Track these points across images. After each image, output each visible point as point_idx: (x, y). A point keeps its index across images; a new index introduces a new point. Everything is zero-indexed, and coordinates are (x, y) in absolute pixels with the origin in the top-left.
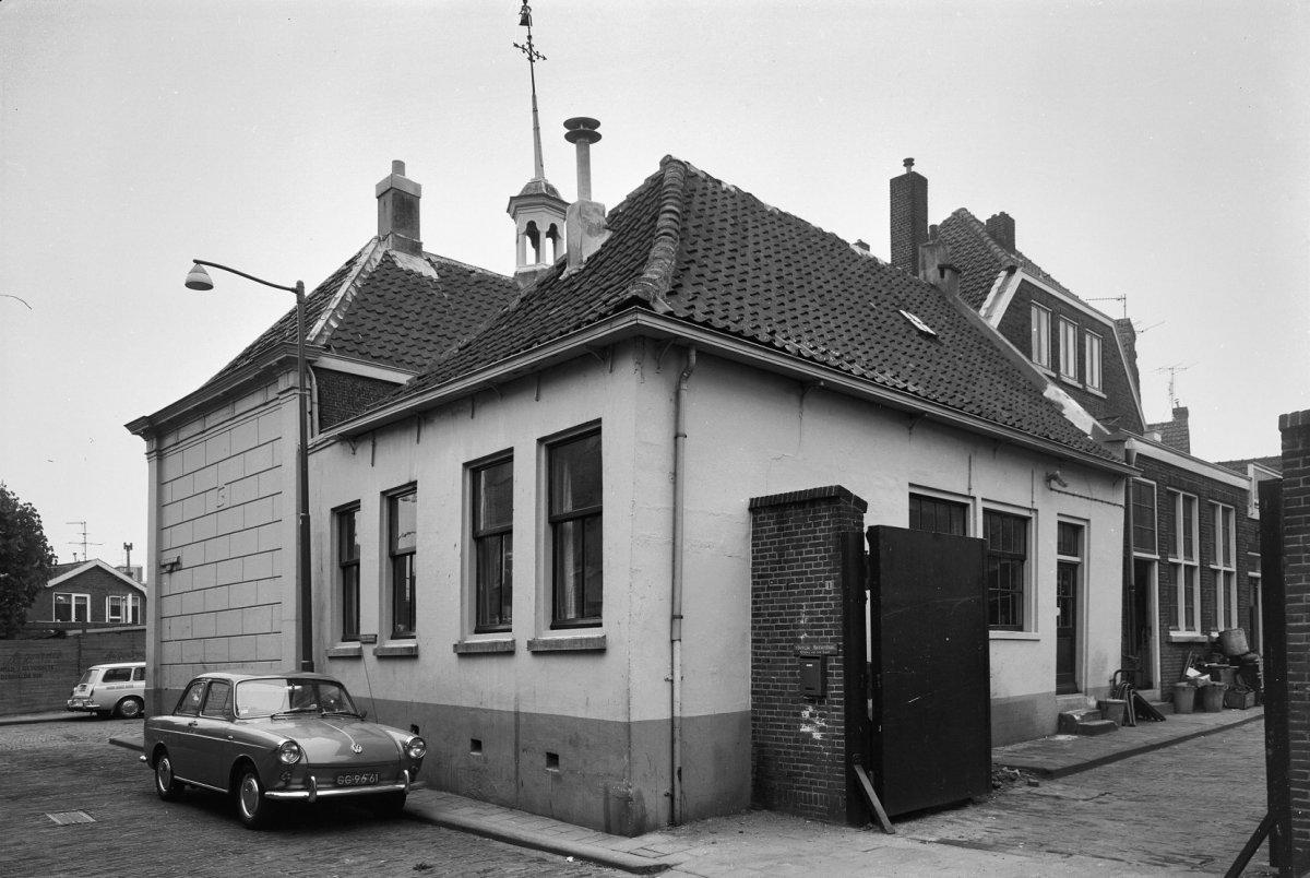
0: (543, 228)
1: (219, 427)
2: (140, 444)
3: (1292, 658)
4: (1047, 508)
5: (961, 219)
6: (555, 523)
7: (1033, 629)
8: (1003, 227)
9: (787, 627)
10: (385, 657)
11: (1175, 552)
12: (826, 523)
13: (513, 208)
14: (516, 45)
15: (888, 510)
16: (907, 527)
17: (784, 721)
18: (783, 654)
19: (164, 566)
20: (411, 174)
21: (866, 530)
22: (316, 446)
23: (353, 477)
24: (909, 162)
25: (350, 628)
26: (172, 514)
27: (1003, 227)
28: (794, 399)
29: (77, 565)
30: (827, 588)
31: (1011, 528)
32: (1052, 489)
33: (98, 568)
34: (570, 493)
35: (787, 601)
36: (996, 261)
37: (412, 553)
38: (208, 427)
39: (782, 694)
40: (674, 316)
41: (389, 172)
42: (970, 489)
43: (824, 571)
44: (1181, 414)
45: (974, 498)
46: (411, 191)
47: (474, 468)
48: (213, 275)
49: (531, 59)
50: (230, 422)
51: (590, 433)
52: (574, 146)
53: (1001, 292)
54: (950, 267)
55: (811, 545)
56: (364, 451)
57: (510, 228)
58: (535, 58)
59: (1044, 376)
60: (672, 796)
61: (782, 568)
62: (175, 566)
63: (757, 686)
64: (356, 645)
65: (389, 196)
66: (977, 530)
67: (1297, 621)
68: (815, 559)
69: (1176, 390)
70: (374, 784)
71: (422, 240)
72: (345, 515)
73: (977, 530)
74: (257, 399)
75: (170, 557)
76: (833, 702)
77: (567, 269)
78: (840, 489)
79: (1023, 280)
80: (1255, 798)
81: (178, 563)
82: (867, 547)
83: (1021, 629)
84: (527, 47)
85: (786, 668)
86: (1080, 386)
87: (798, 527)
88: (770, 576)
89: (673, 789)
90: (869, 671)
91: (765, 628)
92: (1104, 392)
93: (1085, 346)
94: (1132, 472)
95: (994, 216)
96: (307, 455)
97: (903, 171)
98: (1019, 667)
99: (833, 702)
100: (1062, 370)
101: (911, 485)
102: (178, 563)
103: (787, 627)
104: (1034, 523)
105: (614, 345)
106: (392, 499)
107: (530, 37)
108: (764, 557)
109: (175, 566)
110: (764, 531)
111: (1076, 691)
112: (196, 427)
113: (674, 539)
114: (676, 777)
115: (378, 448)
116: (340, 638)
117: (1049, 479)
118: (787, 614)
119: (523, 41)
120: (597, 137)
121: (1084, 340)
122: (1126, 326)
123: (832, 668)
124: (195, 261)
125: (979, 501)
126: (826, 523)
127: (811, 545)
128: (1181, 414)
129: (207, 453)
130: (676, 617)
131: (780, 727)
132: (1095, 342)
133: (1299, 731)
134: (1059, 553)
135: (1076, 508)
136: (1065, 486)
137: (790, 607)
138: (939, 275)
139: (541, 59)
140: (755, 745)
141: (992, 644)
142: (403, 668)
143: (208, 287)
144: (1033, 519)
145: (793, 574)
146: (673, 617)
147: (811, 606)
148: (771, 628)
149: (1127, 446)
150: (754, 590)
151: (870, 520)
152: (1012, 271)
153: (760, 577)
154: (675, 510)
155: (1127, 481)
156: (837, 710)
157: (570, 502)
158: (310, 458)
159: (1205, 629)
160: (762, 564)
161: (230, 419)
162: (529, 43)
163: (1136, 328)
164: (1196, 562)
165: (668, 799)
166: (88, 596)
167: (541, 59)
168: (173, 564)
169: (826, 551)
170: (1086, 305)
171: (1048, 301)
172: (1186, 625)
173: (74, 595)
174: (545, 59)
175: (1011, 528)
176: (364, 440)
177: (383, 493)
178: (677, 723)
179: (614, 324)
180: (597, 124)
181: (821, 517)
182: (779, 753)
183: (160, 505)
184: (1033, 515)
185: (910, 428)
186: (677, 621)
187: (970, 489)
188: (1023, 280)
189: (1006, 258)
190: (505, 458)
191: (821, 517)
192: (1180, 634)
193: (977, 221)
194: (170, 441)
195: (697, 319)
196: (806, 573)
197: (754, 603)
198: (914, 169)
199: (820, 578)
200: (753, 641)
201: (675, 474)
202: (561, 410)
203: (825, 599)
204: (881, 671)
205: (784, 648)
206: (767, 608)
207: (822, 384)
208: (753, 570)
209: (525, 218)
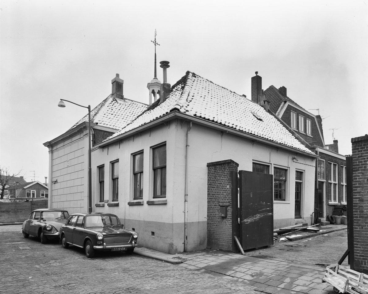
0: (156, 91)
1: (68, 145)
2: (47, 149)
3: (355, 206)
4: (293, 166)
5: (272, 88)
6: (155, 170)
7: (288, 201)
8: (283, 90)
9: (217, 198)
10: (110, 205)
11: (331, 180)
12: (227, 170)
15: (245, 165)
16: (251, 170)
17: (216, 224)
18: (216, 205)
19: (53, 182)
20: (121, 77)
21: (238, 172)
22: (93, 149)
23: (102, 158)
24: (257, 73)
25: (102, 199)
26: (55, 168)
27: (283, 90)
28: (220, 136)
29: (32, 182)
30: (227, 187)
31: (282, 172)
32: (294, 162)
33: (38, 183)
34: (159, 163)
35: (217, 191)
36: (281, 100)
37: (118, 178)
38: (65, 144)
39: (215, 216)
40: (252, 134)
41: (115, 76)
42: (270, 161)
43: (227, 183)
44: (336, 142)
45: (271, 164)
46: (121, 82)
47: (134, 155)
48: (65, 103)
50: (70, 143)
51: (163, 145)
52: (162, 69)
53: (282, 108)
54: (267, 101)
55: (223, 176)
56: (106, 150)
59: (293, 131)
60: (184, 244)
61: (215, 182)
62: (56, 182)
63: (209, 214)
64: (103, 203)
65: (115, 83)
66: (272, 172)
67: (356, 196)
68: (224, 179)
69: (334, 135)
70: (119, 247)
71: (123, 95)
72: (101, 168)
73: (272, 172)
74: (78, 137)
75: (54, 180)
76: (229, 219)
77: (160, 102)
78: (231, 160)
79: (289, 105)
80: (345, 246)
81: (57, 181)
82: (238, 176)
83: (284, 200)
84: (154, 42)
85: (216, 209)
86: (305, 134)
87: (220, 171)
88: (212, 184)
89: (185, 242)
90: (239, 210)
91: (211, 198)
92: (312, 135)
93: (306, 123)
94: (318, 157)
95: (281, 87)
96: (91, 152)
97: (255, 75)
98: (283, 212)
99: (229, 219)
100: (307, 133)
101: (253, 160)
102: (57, 181)
103: (217, 198)
104: (288, 171)
105: (170, 121)
106: (113, 163)
107: (155, 39)
108: (211, 179)
109: (56, 182)
110: (210, 172)
111: (300, 218)
112: (62, 145)
113: (186, 174)
114: (186, 239)
115: (109, 150)
117: (293, 159)
118: (217, 195)
119: (154, 40)
120: (169, 66)
121: (306, 121)
122: (319, 117)
123: (229, 209)
124: (61, 99)
125: (272, 164)
126: (227, 170)
127: (223, 176)
128: (336, 142)
129: (62, 151)
130: (186, 195)
131: (215, 225)
132: (309, 121)
133: (357, 227)
134: (296, 179)
135: (301, 167)
136: (297, 161)
137: (217, 193)
138: (264, 103)
140: (208, 230)
141: (274, 204)
142: (116, 208)
143: (64, 106)
144: (288, 170)
145: (218, 184)
146: (185, 195)
147: (223, 192)
148: (212, 198)
149: (316, 150)
150: (208, 188)
151: (239, 169)
152: (285, 102)
153: (210, 184)
154: (186, 166)
155: (316, 160)
156: (230, 221)
157: (159, 164)
158: (91, 153)
159: (339, 201)
160: (210, 181)
161: (71, 142)
163: (322, 118)
164: (337, 183)
165: (184, 244)
166: (35, 191)
168: (55, 182)
169: (227, 177)
170: (307, 111)
171: (295, 110)
172: (334, 200)
173: (31, 191)
175: (282, 172)
176: (106, 148)
177: (110, 162)
178: (186, 224)
179: (169, 115)
180: (169, 63)
181: (226, 168)
182: (214, 233)
183: (52, 166)
184: (288, 169)
185: (277, 151)
186: (186, 196)
187: (270, 161)
188: (289, 105)
189: (283, 99)
190: (141, 152)
191: (226, 168)
192: (332, 202)
193: (276, 89)
194: (55, 148)
195: (230, 126)
196: (222, 183)
197: (208, 191)
198: (258, 74)
199: (225, 185)
200: (208, 202)
201: (186, 156)
202: (156, 139)
203: (227, 190)
204: (244, 211)
205: (216, 204)
206: (211, 193)
207: (227, 132)
208: (208, 183)
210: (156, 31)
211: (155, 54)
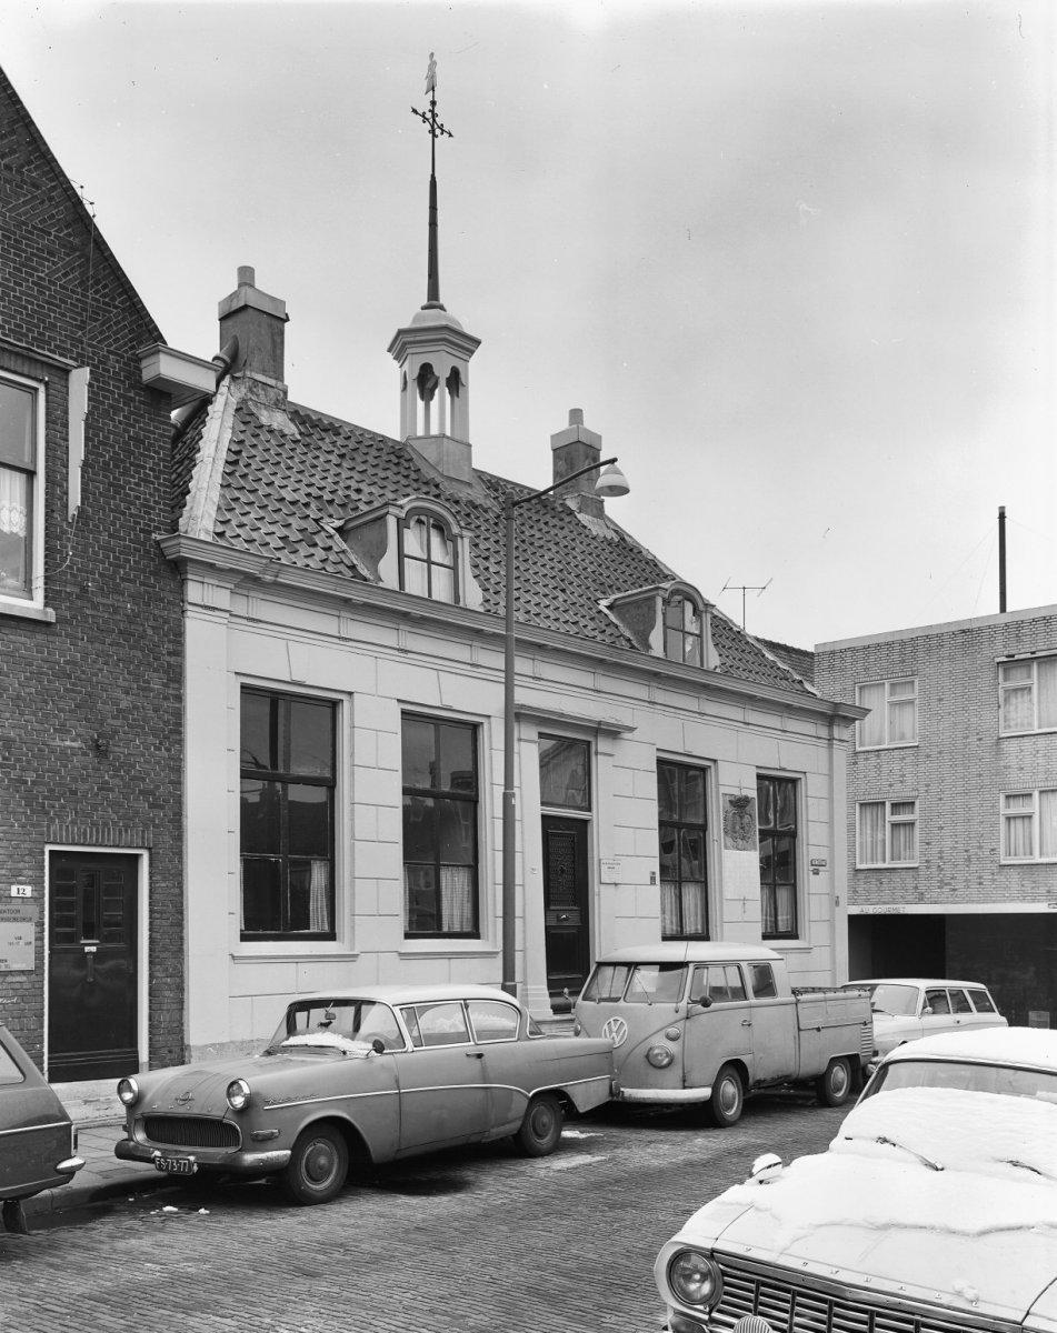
0: (442, 372)
13: (398, 346)
14: (415, 111)
24: (576, 415)
41: (231, 285)
49: (433, 131)
57: (391, 373)
58: (438, 132)
82: (263, 1181)
84: (429, 115)
107: (433, 103)
116: (759, 930)
119: (425, 107)
139: (421, 112)
162: (432, 111)
167: (421, 112)
174: (450, 135)
209: (412, 367)
210: (433, 64)
211: (433, 177)
